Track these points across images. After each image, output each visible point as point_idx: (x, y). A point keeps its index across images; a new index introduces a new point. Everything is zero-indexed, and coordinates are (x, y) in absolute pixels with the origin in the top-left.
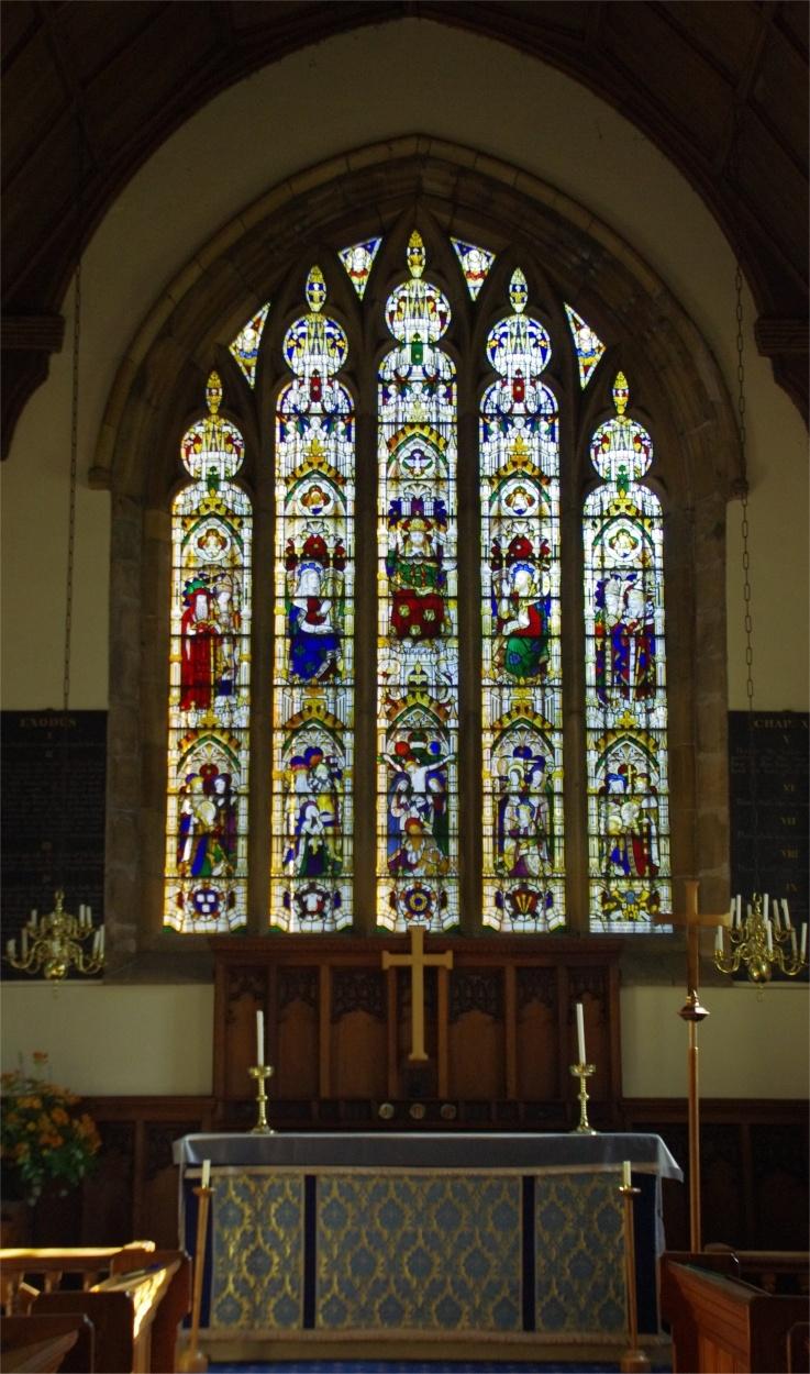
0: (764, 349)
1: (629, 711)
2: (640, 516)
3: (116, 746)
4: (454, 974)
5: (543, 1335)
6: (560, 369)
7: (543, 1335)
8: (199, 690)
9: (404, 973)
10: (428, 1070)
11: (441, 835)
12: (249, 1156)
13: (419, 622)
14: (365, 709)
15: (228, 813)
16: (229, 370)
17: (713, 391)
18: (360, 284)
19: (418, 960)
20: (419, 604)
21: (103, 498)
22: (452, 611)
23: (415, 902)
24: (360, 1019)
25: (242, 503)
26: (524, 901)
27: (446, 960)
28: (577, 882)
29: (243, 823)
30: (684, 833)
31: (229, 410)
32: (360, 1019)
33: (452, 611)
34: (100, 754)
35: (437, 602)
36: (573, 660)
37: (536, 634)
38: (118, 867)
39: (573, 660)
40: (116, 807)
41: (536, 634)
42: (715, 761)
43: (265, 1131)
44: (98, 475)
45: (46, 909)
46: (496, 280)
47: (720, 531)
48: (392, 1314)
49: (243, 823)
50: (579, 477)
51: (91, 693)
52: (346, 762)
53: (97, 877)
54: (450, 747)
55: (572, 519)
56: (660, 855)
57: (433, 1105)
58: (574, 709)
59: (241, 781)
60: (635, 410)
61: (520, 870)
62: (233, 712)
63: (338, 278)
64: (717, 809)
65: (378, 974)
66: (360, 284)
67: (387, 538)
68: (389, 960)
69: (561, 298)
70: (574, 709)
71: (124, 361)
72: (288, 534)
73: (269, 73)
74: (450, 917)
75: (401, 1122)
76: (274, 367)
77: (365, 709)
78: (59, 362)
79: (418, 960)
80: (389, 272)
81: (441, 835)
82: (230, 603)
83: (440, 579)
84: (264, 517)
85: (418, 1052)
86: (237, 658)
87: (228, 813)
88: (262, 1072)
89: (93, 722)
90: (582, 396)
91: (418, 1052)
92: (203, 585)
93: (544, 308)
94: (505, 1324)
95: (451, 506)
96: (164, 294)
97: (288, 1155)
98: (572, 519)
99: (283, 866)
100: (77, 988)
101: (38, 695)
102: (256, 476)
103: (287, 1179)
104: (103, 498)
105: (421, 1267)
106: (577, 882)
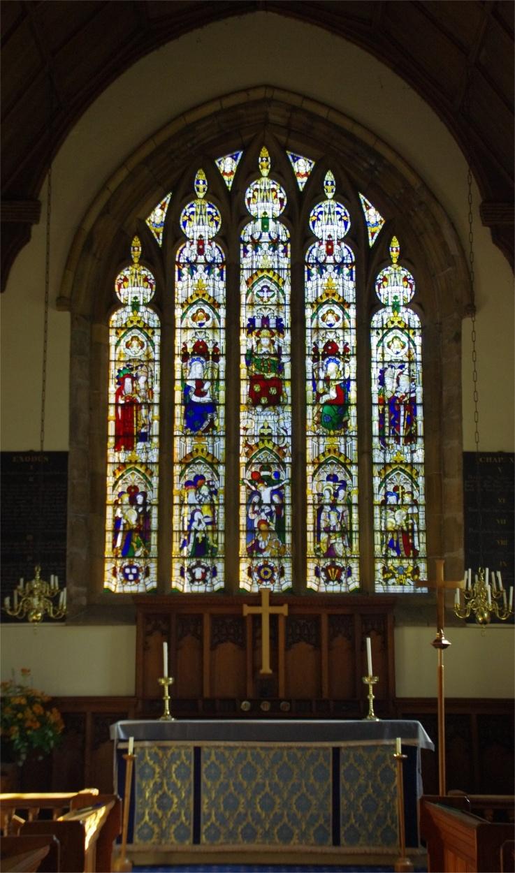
0: (485, 222)
1: (400, 452)
2: (407, 328)
3: (74, 474)
4: (289, 619)
5: (345, 848)
6: (356, 235)
7: (345, 848)
8: (126, 438)
9: (257, 618)
10: (272, 680)
11: (280, 531)
12: (158, 735)
13: (266, 395)
14: (232, 450)
15: (145, 516)
16: (145, 235)
17: (453, 249)
18: (229, 181)
19: (265, 610)
20: (266, 384)
21: (66, 316)
22: (287, 388)
23: (264, 573)
24: (229, 647)
25: (154, 320)
26: (333, 573)
27: (284, 610)
28: (367, 561)
29: (154, 523)
30: (435, 529)
31: (146, 261)
32: (229, 647)
33: (287, 388)
34: (63, 479)
35: (278, 383)
36: (365, 419)
37: (341, 403)
38: (75, 551)
39: (365, 419)
40: (74, 513)
41: (341, 403)
42: (455, 483)
43: (168, 719)
44: (63, 302)
45: (30, 577)
46: (315, 178)
47: (458, 337)
48: (249, 835)
49: (154, 523)
50: (368, 303)
51: (58, 440)
52: (220, 484)
53: (61, 557)
54: (286, 475)
55: (364, 329)
56: (420, 543)
57: (275, 702)
58: (365, 450)
59: (153, 496)
60: (404, 261)
61: (331, 553)
62: (148, 452)
63: (215, 177)
64: (456, 514)
65: (240, 619)
66: (229, 181)
67: (246, 342)
68: (248, 610)
69: (357, 189)
70: (365, 450)
71: (79, 229)
72: (183, 339)
73: (171, 47)
74: (286, 583)
75: (255, 713)
76: (174, 233)
77: (232, 450)
78: (38, 230)
79: (265, 610)
80: (247, 173)
81: (280, 531)
82: (146, 383)
83: (280, 368)
84: (168, 329)
85: (266, 669)
86: (151, 418)
87: (145, 516)
88: (166, 681)
89: (59, 459)
90: (370, 252)
91: (266, 669)
92: (129, 372)
93: (346, 196)
94: (321, 841)
95: (287, 321)
96: (104, 187)
97: (183, 734)
98: (364, 329)
99: (180, 550)
100: (49, 628)
101: (24, 441)
102: (163, 302)
103: (182, 749)
104: (66, 316)
105: (268, 805)
106: (367, 561)
